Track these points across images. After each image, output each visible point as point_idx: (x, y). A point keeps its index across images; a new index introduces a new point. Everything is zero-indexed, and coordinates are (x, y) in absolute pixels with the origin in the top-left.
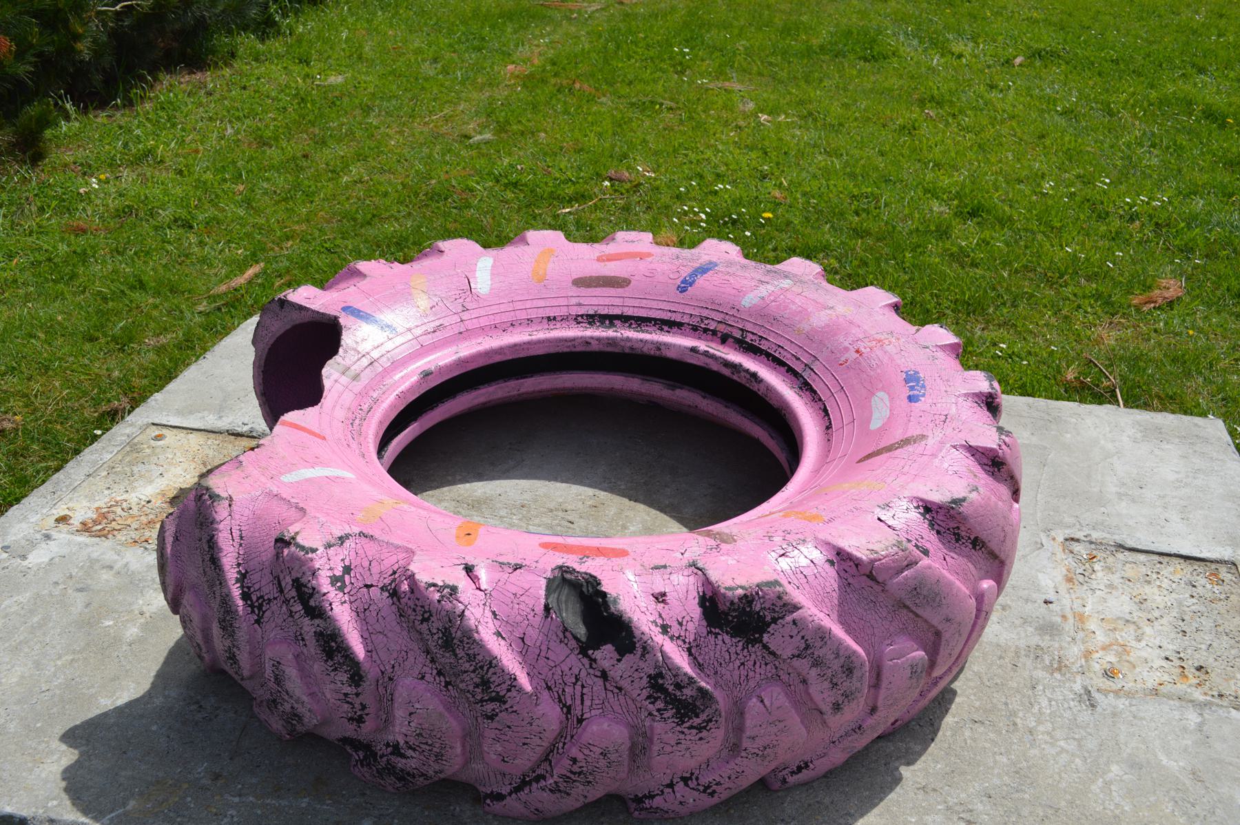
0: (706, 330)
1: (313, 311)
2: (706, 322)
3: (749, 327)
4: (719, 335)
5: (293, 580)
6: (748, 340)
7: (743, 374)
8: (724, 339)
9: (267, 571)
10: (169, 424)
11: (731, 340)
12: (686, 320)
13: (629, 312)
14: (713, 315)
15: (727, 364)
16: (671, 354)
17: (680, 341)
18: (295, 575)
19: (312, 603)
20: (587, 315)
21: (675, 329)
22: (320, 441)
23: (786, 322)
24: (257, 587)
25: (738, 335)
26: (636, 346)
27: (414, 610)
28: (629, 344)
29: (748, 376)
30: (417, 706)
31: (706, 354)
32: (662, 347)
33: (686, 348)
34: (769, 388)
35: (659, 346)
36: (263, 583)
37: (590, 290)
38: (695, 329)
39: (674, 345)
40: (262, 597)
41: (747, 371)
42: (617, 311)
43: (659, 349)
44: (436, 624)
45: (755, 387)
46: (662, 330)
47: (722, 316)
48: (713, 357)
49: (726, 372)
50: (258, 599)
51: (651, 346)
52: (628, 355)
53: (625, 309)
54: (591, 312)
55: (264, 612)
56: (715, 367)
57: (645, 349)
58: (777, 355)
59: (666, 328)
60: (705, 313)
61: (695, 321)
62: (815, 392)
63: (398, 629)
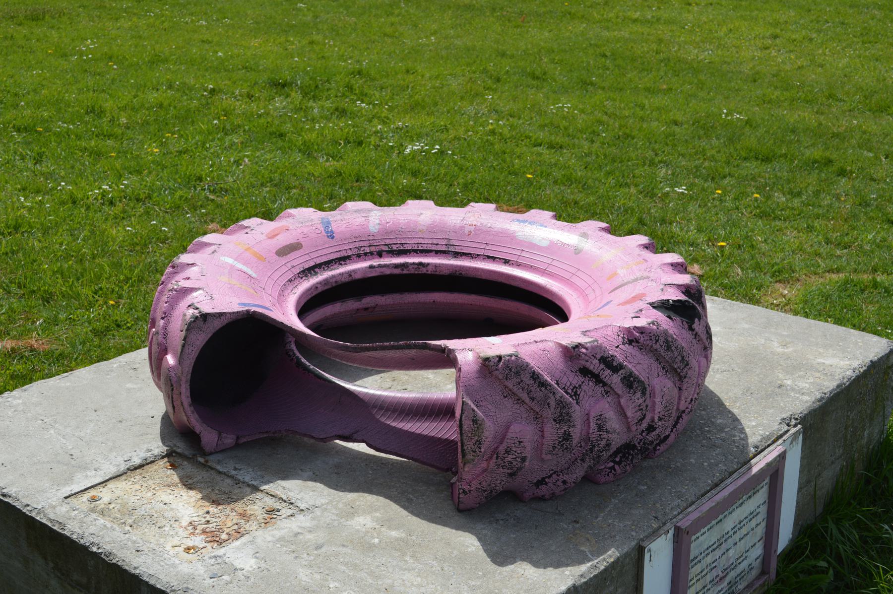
0: (366, 254)
1: (230, 313)
2: (362, 249)
3: (388, 242)
4: (375, 253)
5: (599, 360)
6: (395, 248)
7: (411, 267)
8: (380, 254)
9: (569, 372)
10: (73, 492)
11: (384, 253)
12: (350, 253)
13: (318, 261)
14: (362, 244)
15: (396, 266)
16: (358, 276)
17: (359, 266)
18: (598, 357)
19: (615, 364)
20: (302, 271)
21: (348, 261)
22: (66, 495)
23: (408, 230)
24: (568, 384)
25: (386, 248)
26: (338, 279)
27: (651, 340)
28: (334, 280)
29: (416, 266)
30: (665, 389)
31: (380, 266)
32: (352, 274)
33: (366, 268)
34: (436, 266)
35: (350, 274)
36: (571, 379)
37: (289, 256)
38: (359, 256)
39: (359, 269)
40: (574, 387)
41: (414, 263)
42: (312, 264)
43: (350, 276)
44: (662, 339)
45: (424, 270)
46: (341, 264)
47: (368, 242)
48: (385, 266)
49: (397, 271)
50: (572, 390)
51: (346, 276)
52: (336, 287)
53: (315, 260)
54: (302, 269)
55: (579, 395)
56: (388, 272)
57: (343, 280)
58: (420, 248)
59: (343, 263)
60: (357, 245)
61: (355, 251)
62: (470, 254)
63: (643, 357)
